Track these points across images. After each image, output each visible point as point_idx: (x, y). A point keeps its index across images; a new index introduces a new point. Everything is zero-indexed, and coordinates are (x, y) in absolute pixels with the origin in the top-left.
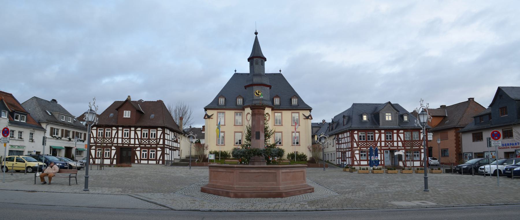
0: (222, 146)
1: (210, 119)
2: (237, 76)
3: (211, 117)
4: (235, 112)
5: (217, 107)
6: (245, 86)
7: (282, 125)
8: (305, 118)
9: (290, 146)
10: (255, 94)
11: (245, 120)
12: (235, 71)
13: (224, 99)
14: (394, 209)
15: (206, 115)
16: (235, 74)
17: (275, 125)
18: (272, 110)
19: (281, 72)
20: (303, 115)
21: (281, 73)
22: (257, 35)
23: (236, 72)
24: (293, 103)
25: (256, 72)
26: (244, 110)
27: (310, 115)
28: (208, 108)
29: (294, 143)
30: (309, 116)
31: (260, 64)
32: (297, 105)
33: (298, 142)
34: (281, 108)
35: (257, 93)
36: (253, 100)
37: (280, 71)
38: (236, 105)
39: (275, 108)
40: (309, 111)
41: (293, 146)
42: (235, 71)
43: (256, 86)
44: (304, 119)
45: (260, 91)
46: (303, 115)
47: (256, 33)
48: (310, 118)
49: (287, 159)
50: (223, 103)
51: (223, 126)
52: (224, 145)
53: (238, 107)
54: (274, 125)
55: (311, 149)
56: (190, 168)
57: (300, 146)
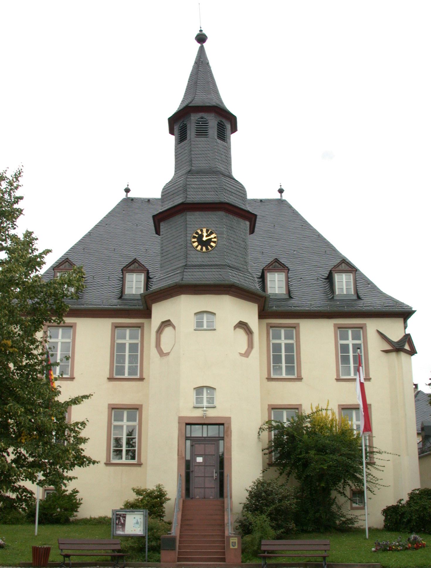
4: (116, 326)
6: (154, 217)
7: (299, 379)
8: (389, 347)
10: (196, 244)
11: (154, 351)
12: (127, 190)
17: (273, 376)
19: (285, 196)
21: (284, 198)
22: (204, 44)
23: (130, 195)
24: (337, 292)
25: (200, 164)
26: (147, 314)
27: (407, 338)
31: (213, 131)
32: (355, 297)
35: (200, 238)
36: (186, 265)
37: (281, 191)
42: (127, 190)
43: (197, 213)
45: (207, 249)
47: (201, 38)
48: (407, 347)
54: (269, 379)
56: (267, 458)
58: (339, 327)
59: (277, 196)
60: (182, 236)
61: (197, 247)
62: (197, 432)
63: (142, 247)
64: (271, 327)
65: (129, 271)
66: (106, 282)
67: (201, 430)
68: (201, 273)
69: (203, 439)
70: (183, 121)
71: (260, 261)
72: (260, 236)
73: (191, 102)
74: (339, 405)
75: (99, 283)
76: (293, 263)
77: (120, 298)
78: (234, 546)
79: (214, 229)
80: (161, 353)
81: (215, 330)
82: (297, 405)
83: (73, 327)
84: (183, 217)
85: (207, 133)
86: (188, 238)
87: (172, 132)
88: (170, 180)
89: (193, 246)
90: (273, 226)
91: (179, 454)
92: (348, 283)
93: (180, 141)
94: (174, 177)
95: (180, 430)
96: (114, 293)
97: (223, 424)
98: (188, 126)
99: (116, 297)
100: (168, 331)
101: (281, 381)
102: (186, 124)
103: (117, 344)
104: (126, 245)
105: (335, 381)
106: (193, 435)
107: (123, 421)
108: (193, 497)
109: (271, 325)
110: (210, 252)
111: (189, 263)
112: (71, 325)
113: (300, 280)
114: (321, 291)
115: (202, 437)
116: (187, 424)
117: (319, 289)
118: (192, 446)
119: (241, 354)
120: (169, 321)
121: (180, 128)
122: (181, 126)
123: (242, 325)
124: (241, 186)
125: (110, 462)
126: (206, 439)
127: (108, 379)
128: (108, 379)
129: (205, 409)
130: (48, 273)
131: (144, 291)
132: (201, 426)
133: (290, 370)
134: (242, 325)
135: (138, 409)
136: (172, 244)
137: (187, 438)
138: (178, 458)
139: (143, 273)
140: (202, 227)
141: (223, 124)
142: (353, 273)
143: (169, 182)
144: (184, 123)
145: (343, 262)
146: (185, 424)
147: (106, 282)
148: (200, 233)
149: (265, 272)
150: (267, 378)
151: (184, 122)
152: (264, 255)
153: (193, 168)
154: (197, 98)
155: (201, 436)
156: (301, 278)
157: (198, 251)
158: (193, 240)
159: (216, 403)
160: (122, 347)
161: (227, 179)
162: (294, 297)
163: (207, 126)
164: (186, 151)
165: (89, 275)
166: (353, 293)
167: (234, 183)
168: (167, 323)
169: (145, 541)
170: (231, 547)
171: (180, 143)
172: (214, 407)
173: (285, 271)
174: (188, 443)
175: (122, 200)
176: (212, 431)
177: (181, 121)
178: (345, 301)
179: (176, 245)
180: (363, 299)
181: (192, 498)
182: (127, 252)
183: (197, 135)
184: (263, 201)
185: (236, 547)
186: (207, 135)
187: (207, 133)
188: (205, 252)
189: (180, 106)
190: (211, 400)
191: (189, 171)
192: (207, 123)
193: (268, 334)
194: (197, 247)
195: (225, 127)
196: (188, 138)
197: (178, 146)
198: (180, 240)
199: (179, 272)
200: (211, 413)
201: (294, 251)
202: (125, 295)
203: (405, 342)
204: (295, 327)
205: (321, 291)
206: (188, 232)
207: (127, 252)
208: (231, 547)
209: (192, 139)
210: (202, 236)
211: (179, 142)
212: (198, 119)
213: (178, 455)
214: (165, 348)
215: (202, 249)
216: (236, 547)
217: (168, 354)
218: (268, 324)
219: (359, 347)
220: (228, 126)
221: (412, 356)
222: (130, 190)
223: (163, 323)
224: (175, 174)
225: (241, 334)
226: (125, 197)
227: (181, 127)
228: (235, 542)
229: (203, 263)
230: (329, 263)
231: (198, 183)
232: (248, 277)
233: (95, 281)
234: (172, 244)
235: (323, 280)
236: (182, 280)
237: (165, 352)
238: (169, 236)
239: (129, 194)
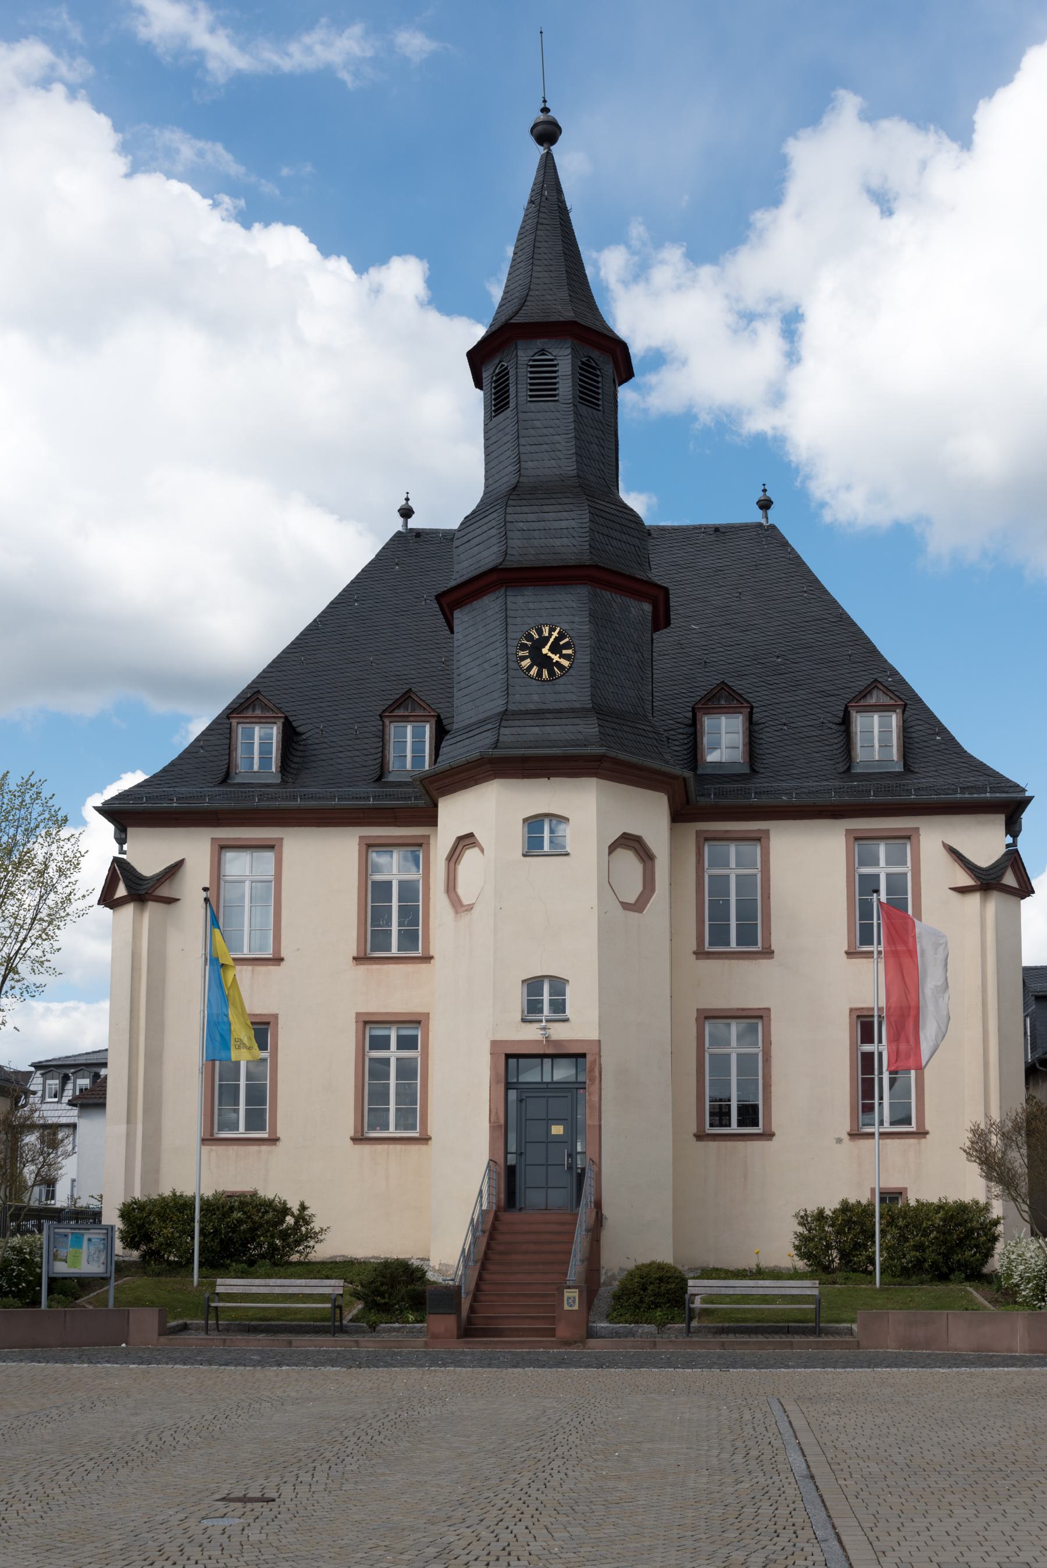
0: (253, 1149)
1: (151, 906)
2: (399, 532)
3: (164, 891)
5: (211, 797)
6: (439, 598)
9: (839, 1141)
13: (275, 731)
14: (479, 531)
15: (119, 870)
16: (399, 538)
17: (707, 948)
18: (678, 816)
19: (775, 517)
20: (955, 854)
23: (414, 523)
26: (430, 818)
27: (1013, 859)
28: (131, 805)
29: (720, 1115)
30: (998, 868)
32: (899, 768)
33: (755, 1108)
34: (754, 800)
37: (765, 505)
38: (227, 775)
39: (702, 801)
40: (1000, 819)
41: (713, 1145)
42: (406, 513)
44: (962, 890)
45: (529, 637)
46: (955, 854)
48: (1010, 879)
49: (801, 1264)
50: (265, 760)
51: (262, 969)
52: (274, 1140)
53: (388, 796)
55: (1018, 1159)
57: (280, 1144)
58: (857, 838)
59: (756, 516)
60: (498, 644)
61: (530, 668)
62: (531, 1075)
63: (433, 656)
64: (706, 839)
65: (397, 719)
66: (350, 743)
67: (540, 1067)
68: (536, 730)
69: (545, 1086)
70: (500, 362)
71: (696, 685)
72: (705, 621)
73: (511, 318)
74: (851, 1010)
75: (333, 744)
76: (772, 687)
77: (379, 779)
78: (571, 1306)
79: (566, 627)
80: (457, 904)
81: (567, 854)
82: (759, 1009)
83: (276, 847)
84: (499, 601)
85: (555, 390)
86: (512, 650)
87: (478, 383)
88: (473, 507)
89: (521, 668)
90: (738, 595)
91: (492, 1119)
92: (885, 732)
93: (495, 411)
94: (482, 500)
95: (494, 1067)
96: (366, 769)
97: (583, 1056)
98: (510, 374)
99: (370, 777)
100: (470, 855)
101: (726, 958)
102: (506, 368)
103: (373, 883)
104: (398, 651)
105: (845, 955)
106: (523, 1078)
107: (389, 1049)
108: (523, 1206)
109: (706, 835)
110: (557, 680)
111: (511, 707)
112: (272, 843)
113: (781, 727)
114: (825, 754)
115: (542, 1083)
116: (508, 1056)
117: (821, 749)
118: (520, 1101)
119: (625, 906)
120: (471, 835)
121: (494, 378)
122: (497, 371)
123: (629, 842)
124: (630, 518)
125: (362, 1135)
126: (550, 1086)
127: (354, 958)
128: (354, 958)
129: (544, 1024)
130: (220, 724)
131: (430, 766)
132: (539, 1060)
133: (255, 1121)
134: (629, 842)
135: (909, 838)
136: (478, 662)
137: (508, 1086)
138: (490, 1126)
139: (428, 722)
140: (542, 622)
141: (594, 365)
142: (898, 711)
143: (472, 514)
144: (503, 365)
145: (876, 686)
146: (503, 1057)
147: (350, 743)
148: (546, 634)
149: (699, 715)
150: (694, 953)
151: (503, 363)
152: (706, 670)
153: (522, 479)
154: (532, 303)
155: (540, 1080)
156: (785, 724)
157: (532, 678)
158: (521, 654)
159: (569, 1012)
160: (382, 889)
161: (597, 506)
162: (762, 771)
163: (555, 372)
164: (509, 437)
165: (311, 727)
166: (895, 758)
167: (616, 513)
168: (466, 841)
169: (875, 1222)
170: (566, 1307)
171: (494, 417)
172: (566, 1020)
173: (743, 710)
174: (513, 1094)
175: (395, 536)
176: (563, 1072)
177: (497, 361)
178: (878, 778)
179: (486, 665)
180: (916, 770)
181: (521, 1209)
182: (399, 669)
183: (531, 396)
184: (721, 530)
185: (576, 1307)
186: (555, 396)
187: (555, 390)
188: (547, 681)
189: (494, 320)
190: (559, 1007)
191: (514, 489)
192: (555, 366)
193: (699, 856)
194: (530, 668)
195: (598, 373)
196: (512, 404)
197: (491, 425)
198: (492, 654)
199: (490, 726)
200: (560, 1032)
201: (778, 657)
202: (389, 772)
203: (1006, 868)
204: (762, 838)
205: (825, 754)
206: (510, 635)
207: (399, 669)
208: (566, 1307)
209: (520, 408)
210: (544, 641)
211: (493, 414)
212: (532, 356)
213: (490, 1122)
214: (465, 891)
215: (540, 674)
216: (576, 1307)
217: (470, 908)
218: (698, 833)
219: (875, 888)
220: (608, 369)
221: (1023, 898)
222: (413, 513)
223: (460, 839)
224: (485, 494)
225: (628, 860)
226: (400, 528)
227: (497, 375)
228: (574, 1298)
229: (545, 707)
230: (853, 684)
231: (531, 517)
232: (644, 733)
233: (326, 740)
234: (478, 662)
235: (834, 726)
236: (495, 747)
237: (465, 902)
238: (472, 643)
239: (409, 520)
